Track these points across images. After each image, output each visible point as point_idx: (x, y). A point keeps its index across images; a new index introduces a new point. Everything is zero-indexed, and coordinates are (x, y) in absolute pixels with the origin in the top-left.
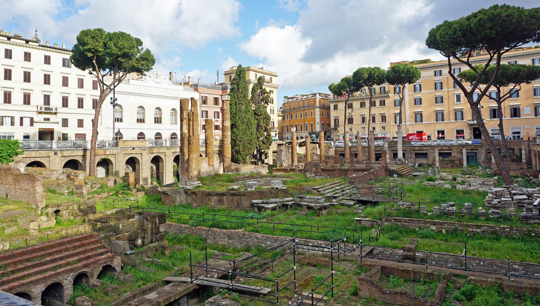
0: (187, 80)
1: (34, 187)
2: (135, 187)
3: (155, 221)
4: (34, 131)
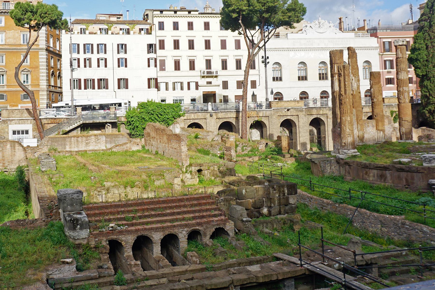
0: (362, 25)
1: (180, 146)
2: (288, 153)
3: (283, 191)
4: (199, 94)
